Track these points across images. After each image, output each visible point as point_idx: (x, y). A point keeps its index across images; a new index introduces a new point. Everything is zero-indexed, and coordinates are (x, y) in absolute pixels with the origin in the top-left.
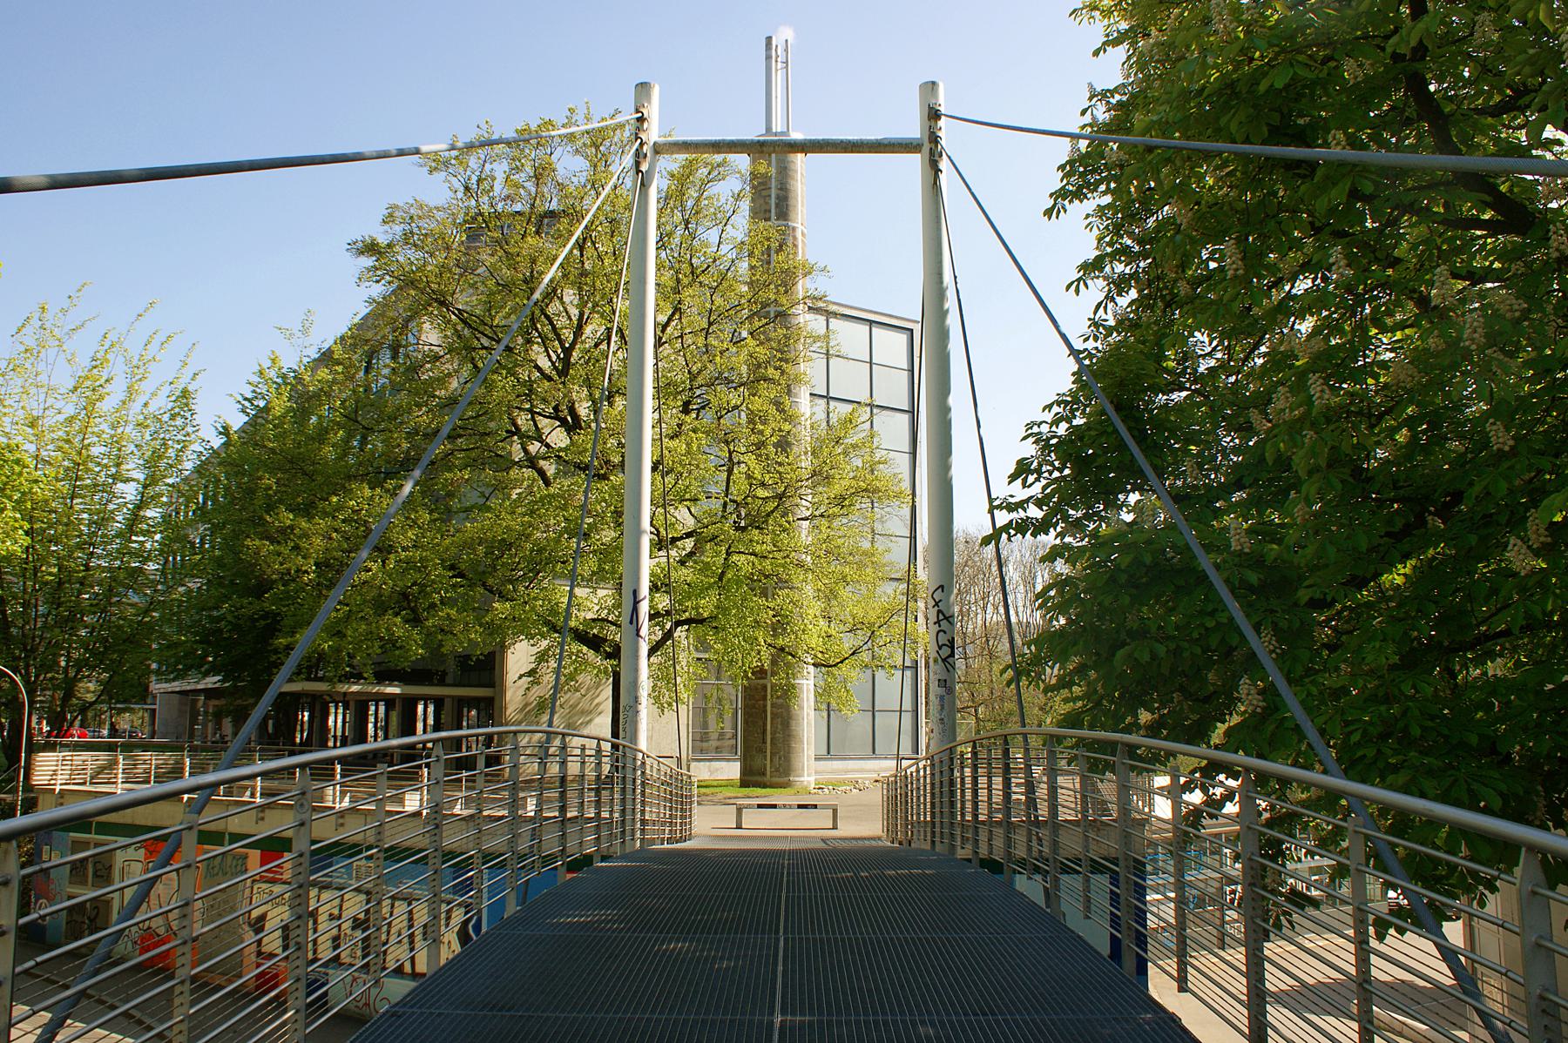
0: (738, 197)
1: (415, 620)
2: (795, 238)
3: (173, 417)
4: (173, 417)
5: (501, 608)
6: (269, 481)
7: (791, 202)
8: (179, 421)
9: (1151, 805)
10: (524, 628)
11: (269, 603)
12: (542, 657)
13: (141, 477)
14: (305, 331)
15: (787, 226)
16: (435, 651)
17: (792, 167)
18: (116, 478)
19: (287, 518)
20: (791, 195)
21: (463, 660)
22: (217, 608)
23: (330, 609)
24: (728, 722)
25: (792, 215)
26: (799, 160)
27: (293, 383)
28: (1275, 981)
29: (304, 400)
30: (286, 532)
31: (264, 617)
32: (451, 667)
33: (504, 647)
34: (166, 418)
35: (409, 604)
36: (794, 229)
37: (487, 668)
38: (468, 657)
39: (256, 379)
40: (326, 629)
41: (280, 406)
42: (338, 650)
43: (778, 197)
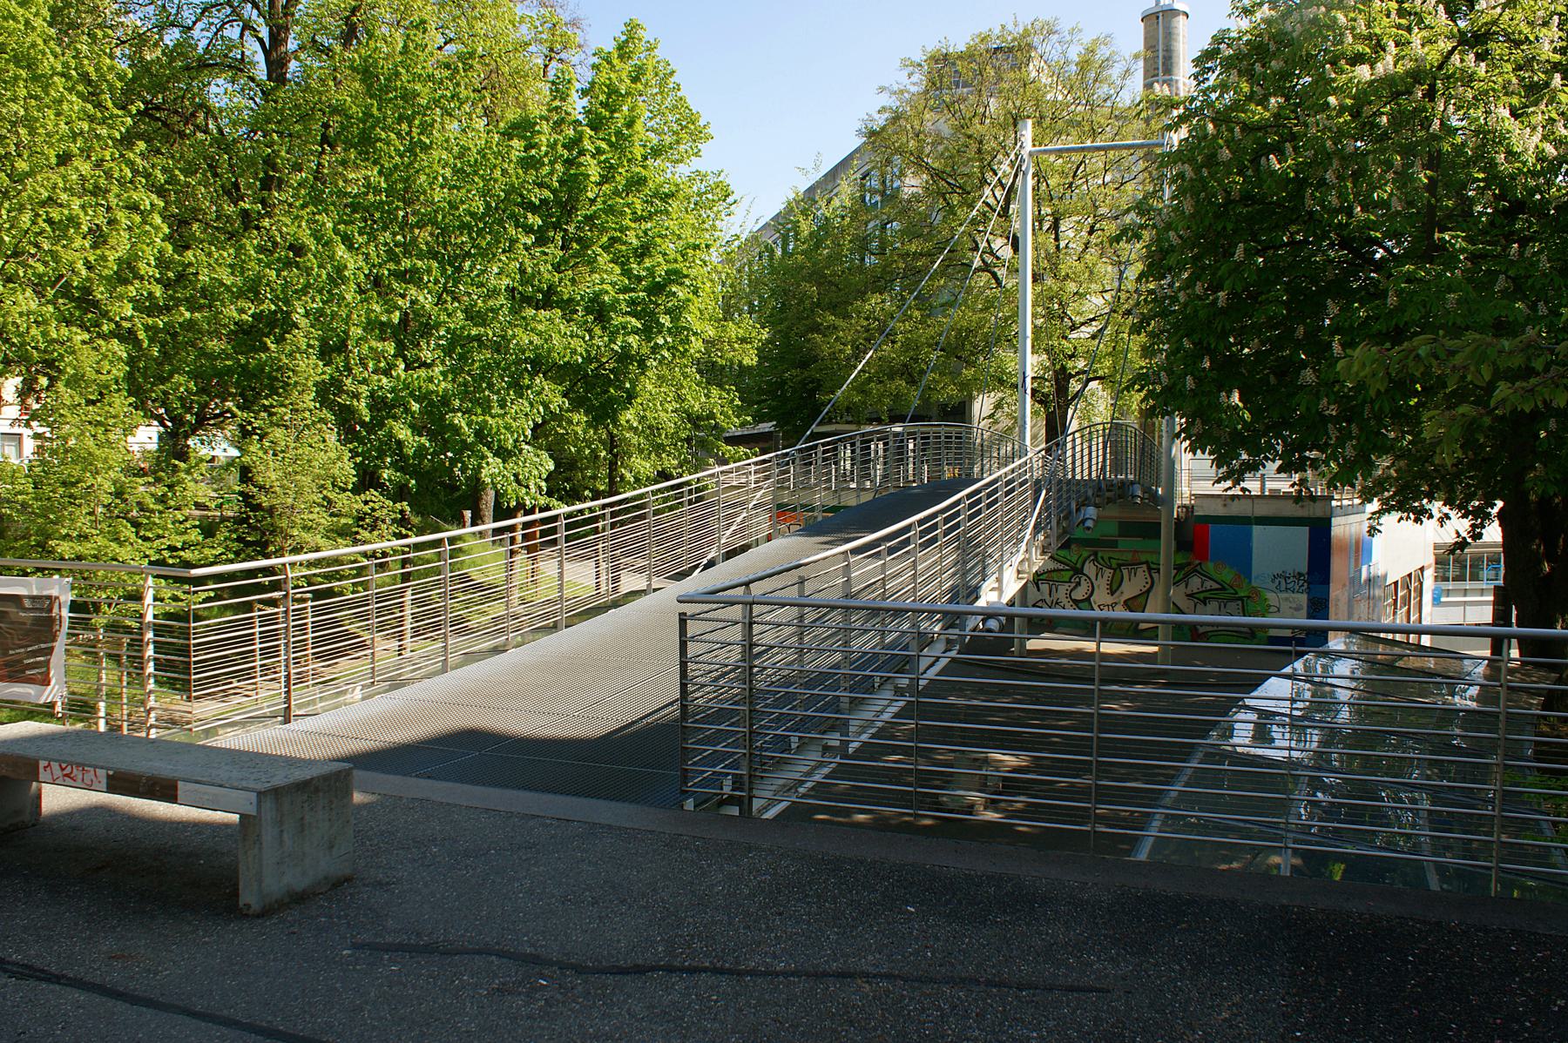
0: (1136, 57)
1: (912, 382)
2: (1177, 88)
5: (968, 373)
7: (1174, 60)
10: (984, 388)
11: (813, 371)
12: (998, 406)
15: (1171, 80)
16: (925, 401)
17: (1175, 31)
20: (1175, 55)
21: (943, 407)
24: (1337, 566)
25: (1175, 70)
26: (1257, 530)
28: (807, 610)
31: (812, 382)
32: (935, 411)
33: (971, 399)
35: (910, 373)
36: (1177, 81)
37: (959, 412)
38: (946, 405)
42: (864, 403)
43: (1164, 57)
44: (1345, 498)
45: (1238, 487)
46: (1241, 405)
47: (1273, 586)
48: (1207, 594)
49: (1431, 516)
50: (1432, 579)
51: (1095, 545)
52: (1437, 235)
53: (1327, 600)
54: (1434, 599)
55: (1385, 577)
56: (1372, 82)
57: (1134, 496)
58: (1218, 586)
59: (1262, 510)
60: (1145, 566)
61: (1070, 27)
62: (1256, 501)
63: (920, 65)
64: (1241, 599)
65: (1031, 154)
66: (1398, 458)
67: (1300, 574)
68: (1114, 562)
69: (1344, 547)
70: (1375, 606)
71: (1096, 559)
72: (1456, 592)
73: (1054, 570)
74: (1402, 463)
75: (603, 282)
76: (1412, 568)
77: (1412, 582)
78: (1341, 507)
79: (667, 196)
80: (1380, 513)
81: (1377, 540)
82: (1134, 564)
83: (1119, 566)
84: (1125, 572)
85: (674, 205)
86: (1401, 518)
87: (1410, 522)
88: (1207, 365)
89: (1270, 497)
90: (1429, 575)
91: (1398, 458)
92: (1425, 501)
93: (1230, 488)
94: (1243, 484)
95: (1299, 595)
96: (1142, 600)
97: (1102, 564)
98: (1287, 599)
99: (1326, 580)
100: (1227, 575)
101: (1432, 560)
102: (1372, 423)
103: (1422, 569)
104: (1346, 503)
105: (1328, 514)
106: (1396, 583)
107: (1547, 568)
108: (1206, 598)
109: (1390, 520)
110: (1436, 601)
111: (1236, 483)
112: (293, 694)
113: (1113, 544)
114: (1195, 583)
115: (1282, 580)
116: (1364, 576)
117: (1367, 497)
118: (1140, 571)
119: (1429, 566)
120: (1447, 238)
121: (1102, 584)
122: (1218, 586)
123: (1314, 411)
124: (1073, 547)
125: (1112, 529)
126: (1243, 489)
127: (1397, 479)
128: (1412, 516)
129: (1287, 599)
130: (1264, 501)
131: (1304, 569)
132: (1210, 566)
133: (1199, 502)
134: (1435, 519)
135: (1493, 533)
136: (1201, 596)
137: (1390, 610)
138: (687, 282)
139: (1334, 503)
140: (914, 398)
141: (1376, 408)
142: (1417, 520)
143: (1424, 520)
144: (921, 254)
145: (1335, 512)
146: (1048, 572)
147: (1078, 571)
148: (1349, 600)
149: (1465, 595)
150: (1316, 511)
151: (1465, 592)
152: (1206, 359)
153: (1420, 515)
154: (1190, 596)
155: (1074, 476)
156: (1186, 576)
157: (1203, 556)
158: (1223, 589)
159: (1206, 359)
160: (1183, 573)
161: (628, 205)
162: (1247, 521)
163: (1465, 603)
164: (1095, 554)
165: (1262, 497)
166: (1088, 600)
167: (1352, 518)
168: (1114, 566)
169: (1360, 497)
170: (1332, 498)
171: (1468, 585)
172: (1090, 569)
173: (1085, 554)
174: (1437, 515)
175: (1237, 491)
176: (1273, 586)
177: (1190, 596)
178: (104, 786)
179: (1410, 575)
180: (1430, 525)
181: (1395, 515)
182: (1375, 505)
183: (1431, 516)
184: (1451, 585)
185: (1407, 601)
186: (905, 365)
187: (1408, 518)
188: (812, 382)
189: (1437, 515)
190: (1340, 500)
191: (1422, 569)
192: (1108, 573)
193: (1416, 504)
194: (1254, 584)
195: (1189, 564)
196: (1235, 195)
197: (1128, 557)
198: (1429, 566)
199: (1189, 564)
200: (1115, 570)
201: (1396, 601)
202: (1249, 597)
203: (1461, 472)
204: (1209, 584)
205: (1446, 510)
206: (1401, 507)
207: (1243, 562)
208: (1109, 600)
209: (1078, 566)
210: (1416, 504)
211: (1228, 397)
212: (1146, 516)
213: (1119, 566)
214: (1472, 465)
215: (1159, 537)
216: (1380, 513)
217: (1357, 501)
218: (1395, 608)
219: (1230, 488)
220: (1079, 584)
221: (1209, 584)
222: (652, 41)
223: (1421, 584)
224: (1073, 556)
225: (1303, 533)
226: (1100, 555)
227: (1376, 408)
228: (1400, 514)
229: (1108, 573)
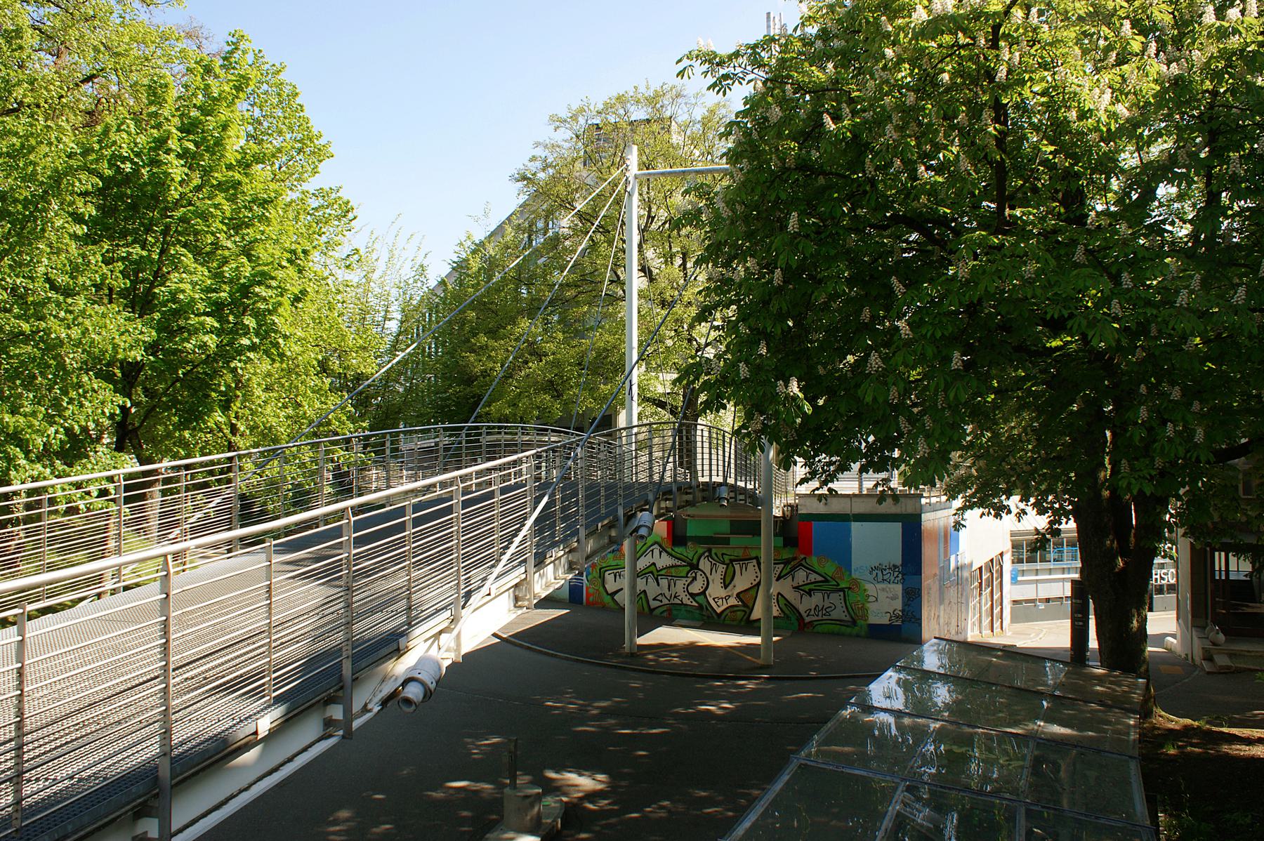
1: (558, 396)
3: (415, 282)
4: (415, 282)
6: (472, 315)
8: (419, 284)
9: (894, 51)
13: (399, 317)
14: (486, 214)
18: (385, 319)
19: (483, 339)
22: (445, 392)
23: (513, 388)
26: (855, 526)
27: (478, 248)
29: (491, 265)
30: (484, 348)
34: (411, 281)
35: (554, 388)
39: (457, 249)
40: (507, 402)
41: (475, 264)
44: (932, 497)
45: (825, 488)
46: (801, 395)
47: (871, 577)
48: (812, 586)
49: (1009, 512)
50: (1010, 561)
51: (710, 542)
52: (1007, 211)
53: (920, 590)
54: (1012, 579)
55: (971, 565)
56: (929, 22)
57: (720, 499)
58: (820, 579)
59: (859, 508)
60: (755, 561)
61: (695, 92)
62: (853, 500)
63: (565, 121)
64: (842, 590)
65: (636, 177)
66: (977, 457)
67: (895, 566)
68: (727, 559)
69: (934, 534)
70: (963, 589)
71: (710, 555)
72: (1029, 572)
73: (673, 566)
74: (982, 463)
75: (181, 281)
76: (993, 554)
77: (994, 566)
78: (930, 504)
79: (265, 201)
80: (963, 509)
81: (963, 532)
82: (745, 559)
83: (732, 561)
84: (737, 567)
85: (272, 214)
86: (983, 514)
87: (991, 517)
88: (764, 351)
89: (867, 495)
90: (1008, 558)
91: (977, 457)
92: (1004, 497)
93: (817, 489)
94: (830, 485)
95: (895, 586)
96: (753, 592)
97: (717, 560)
98: (883, 590)
99: (918, 572)
100: (829, 569)
101: (1009, 546)
102: (947, 414)
103: (1001, 554)
104: (934, 500)
105: (918, 512)
106: (980, 569)
107: (1120, 563)
108: (810, 590)
109: (973, 515)
110: (1014, 581)
111: (825, 483)
112: (172, 644)
113: (726, 541)
114: (801, 576)
115: (879, 571)
116: (953, 565)
117: (952, 493)
118: (750, 566)
119: (1007, 551)
120: (1018, 214)
121: (716, 579)
122: (820, 579)
123: (881, 400)
124: (689, 544)
125: (724, 527)
126: (830, 490)
127: (977, 478)
128: (993, 512)
129: (883, 590)
130: (861, 500)
131: (899, 561)
132: (813, 560)
133: (802, 501)
134: (1013, 514)
135: (1069, 526)
136: (807, 588)
137: (976, 592)
138: (274, 283)
139: (923, 501)
140: (557, 409)
141: (952, 395)
142: (997, 516)
143: (1004, 515)
144: (568, 285)
145: (924, 509)
146: (667, 568)
147: (694, 567)
148: (940, 587)
149: (1037, 575)
150: (906, 507)
151: (1037, 572)
152: (763, 344)
153: (1000, 511)
154: (797, 588)
155: (662, 478)
156: (793, 569)
157: (809, 552)
158: (826, 581)
159: (763, 344)
160: (789, 566)
161: (216, 206)
162: (845, 518)
163: (1037, 581)
164: (710, 550)
165: (860, 496)
166: (704, 593)
167: (940, 514)
168: (727, 561)
169: (945, 494)
170: (921, 496)
171: (1039, 565)
172: (705, 564)
173: (700, 551)
174: (1014, 511)
175: (824, 491)
176: (871, 577)
177: (797, 588)
178: (756, 538)
179: (992, 560)
180: (1008, 522)
181: (977, 511)
182: (958, 503)
183: (1009, 512)
184: (1025, 566)
185: (990, 583)
186: (551, 382)
187: (989, 513)
188: (473, 397)
189: (1014, 511)
190: (929, 497)
191: (1001, 554)
192: (721, 568)
193: (996, 501)
194: (854, 576)
195: (795, 559)
196: (790, 162)
197: (740, 553)
198: (1007, 551)
199: (795, 559)
200: (728, 565)
201: (981, 584)
202: (849, 588)
203: (1035, 470)
204: (813, 577)
205: (1022, 505)
206: (981, 504)
207: (843, 556)
208: (723, 593)
209: (695, 561)
210: (996, 501)
211: (786, 387)
212: (749, 515)
213: (732, 561)
214: (1045, 462)
215: (760, 535)
216: (963, 509)
217: (944, 498)
218: (981, 590)
219: (817, 489)
220: (695, 578)
221: (813, 577)
222: (277, 65)
223: (1001, 567)
224: (689, 552)
225: (897, 527)
226: (714, 551)
227: (952, 395)
228: (981, 510)
229: (721, 568)
